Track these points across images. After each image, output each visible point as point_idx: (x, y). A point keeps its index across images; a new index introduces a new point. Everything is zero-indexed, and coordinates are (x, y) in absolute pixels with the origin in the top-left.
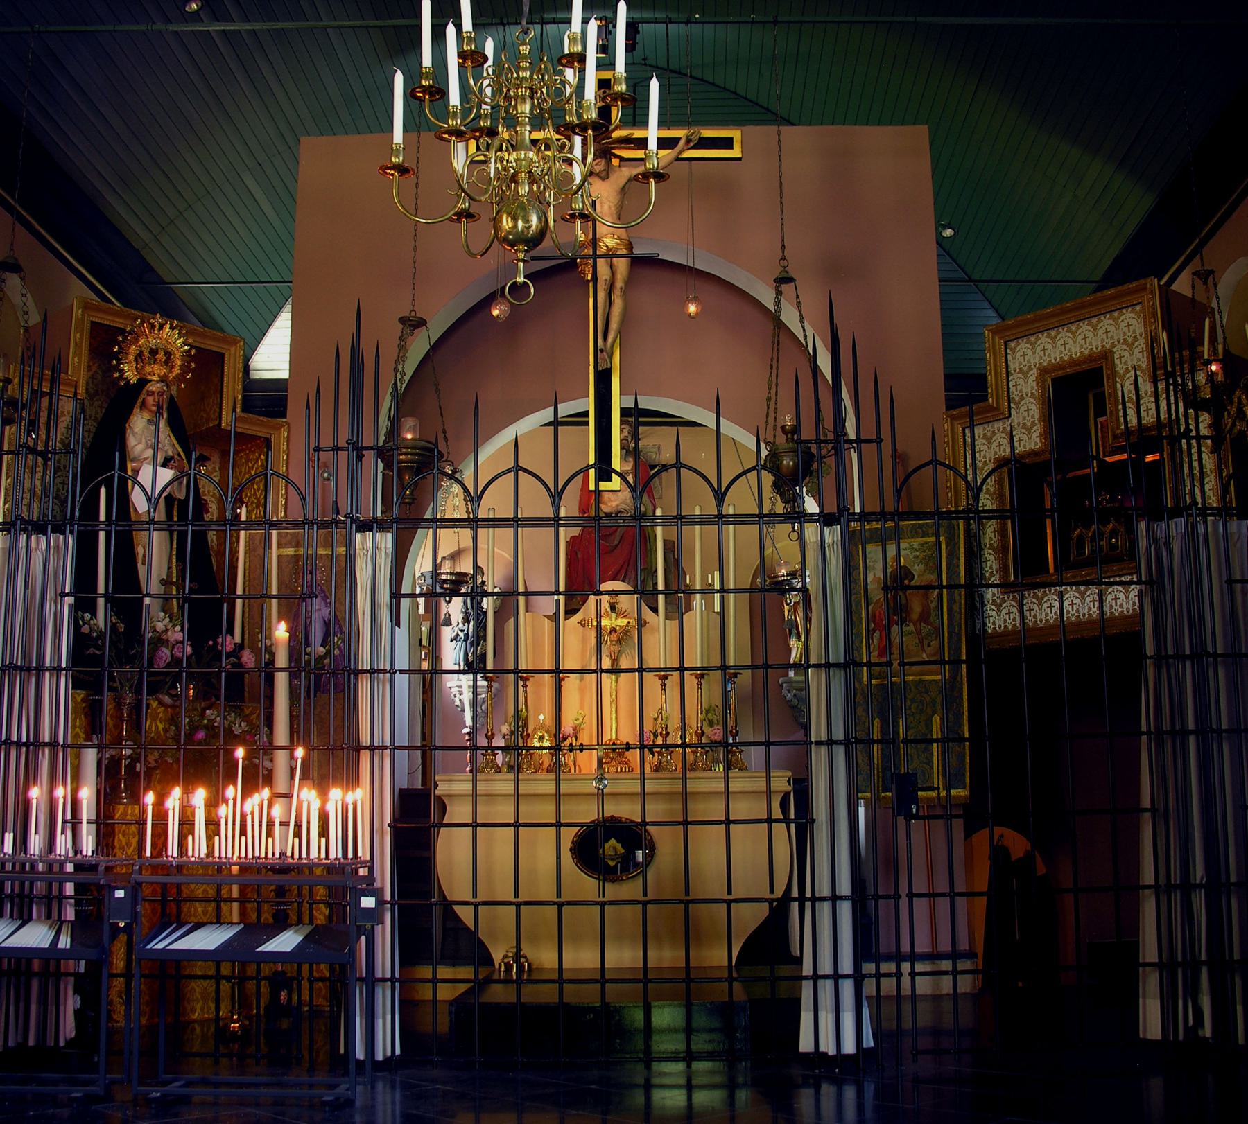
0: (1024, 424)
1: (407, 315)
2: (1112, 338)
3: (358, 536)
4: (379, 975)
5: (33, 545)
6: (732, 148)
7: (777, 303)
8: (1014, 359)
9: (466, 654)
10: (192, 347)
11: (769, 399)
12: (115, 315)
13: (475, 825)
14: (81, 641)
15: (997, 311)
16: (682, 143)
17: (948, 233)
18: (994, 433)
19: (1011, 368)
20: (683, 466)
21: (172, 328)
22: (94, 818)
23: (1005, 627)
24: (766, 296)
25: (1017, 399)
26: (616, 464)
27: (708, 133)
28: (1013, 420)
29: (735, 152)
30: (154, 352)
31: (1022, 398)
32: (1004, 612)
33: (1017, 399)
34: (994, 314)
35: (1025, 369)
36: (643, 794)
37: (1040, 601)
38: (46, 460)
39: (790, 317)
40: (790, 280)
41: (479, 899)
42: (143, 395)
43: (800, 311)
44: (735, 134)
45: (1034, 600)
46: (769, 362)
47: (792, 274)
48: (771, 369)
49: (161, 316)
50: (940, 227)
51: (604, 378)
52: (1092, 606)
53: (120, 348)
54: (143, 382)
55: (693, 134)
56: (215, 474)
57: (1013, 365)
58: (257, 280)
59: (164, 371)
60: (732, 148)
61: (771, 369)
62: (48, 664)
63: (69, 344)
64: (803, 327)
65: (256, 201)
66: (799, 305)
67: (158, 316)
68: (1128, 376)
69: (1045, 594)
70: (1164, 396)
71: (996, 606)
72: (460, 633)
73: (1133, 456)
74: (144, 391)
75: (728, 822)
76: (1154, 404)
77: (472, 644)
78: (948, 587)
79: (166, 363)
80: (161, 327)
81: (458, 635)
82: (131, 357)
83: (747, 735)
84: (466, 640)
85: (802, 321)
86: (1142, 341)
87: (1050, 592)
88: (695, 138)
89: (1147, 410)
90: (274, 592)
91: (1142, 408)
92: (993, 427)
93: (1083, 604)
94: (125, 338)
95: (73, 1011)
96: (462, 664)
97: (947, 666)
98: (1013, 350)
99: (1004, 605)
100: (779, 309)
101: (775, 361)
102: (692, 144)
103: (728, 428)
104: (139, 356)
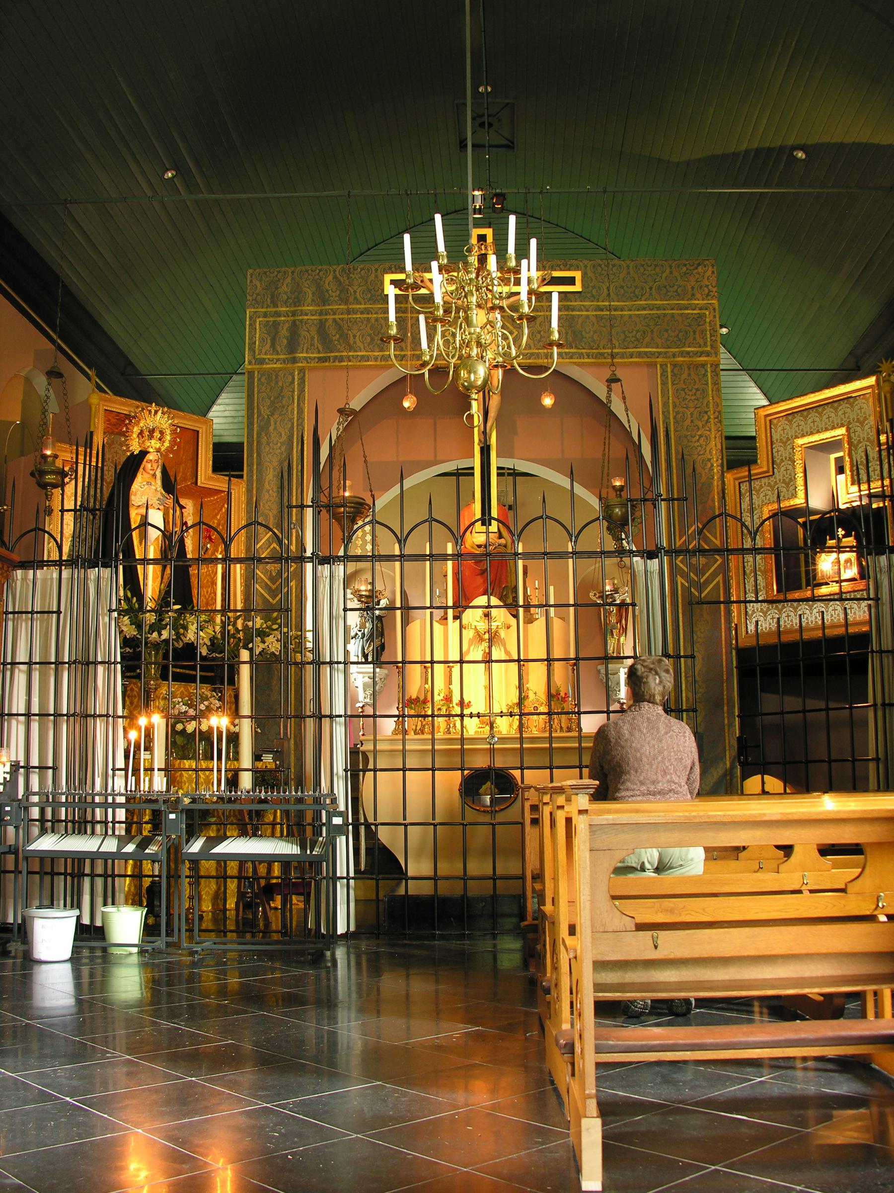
0: (784, 480)
1: (343, 407)
2: (849, 418)
3: (320, 567)
4: (338, 875)
6: (575, 285)
7: (609, 397)
8: (776, 432)
9: (363, 648)
11: (603, 466)
12: (123, 406)
13: (404, 770)
14: (551, 696)
18: (761, 487)
19: (774, 439)
20: (548, 517)
21: (163, 413)
22: (163, 767)
23: (770, 628)
24: (600, 391)
25: (778, 461)
26: (494, 513)
27: (556, 274)
28: (775, 478)
29: (578, 288)
30: (152, 432)
31: (782, 461)
32: (769, 617)
33: (778, 461)
34: (759, 391)
35: (784, 440)
36: (433, 751)
38: (94, 515)
39: (617, 407)
40: (618, 380)
42: (144, 463)
43: (625, 403)
44: (578, 275)
45: (791, 609)
46: (603, 441)
47: (619, 376)
48: (605, 445)
49: (156, 405)
51: (485, 451)
53: (127, 428)
54: (144, 453)
55: (546, 275)
56: (189, 518)
58: (207, 372)
59: (158, 445)
60: (575, 285)
61: (605, 445)
64: (627, 414)
65: (208, 312)
66: (624, 398)
67: (154, 404)
68: (860, 445)
70: (886, 461)
71: (763, 613)
72: (358, 632)
74: (145, 460)
75: (830, 761)
76: (879, 466)
77: (367, 641)
79: (160, 439)
80: (156, 412)
81: (357, 634)
82: (135, 436)
84: (362, 638)
85: (626, 410)
86: (872, 418)
89: (874, 470)
91: (870, 469)
92: (761, 482)
93: (811, 614)
94: (131, 421)
96: (360, 655)
98: (776, 425)
99: (769, 613)
100: (610, 402)
101: (607, 439)
102: (545, 282)
103: (579, 490)
104: (141, 433)
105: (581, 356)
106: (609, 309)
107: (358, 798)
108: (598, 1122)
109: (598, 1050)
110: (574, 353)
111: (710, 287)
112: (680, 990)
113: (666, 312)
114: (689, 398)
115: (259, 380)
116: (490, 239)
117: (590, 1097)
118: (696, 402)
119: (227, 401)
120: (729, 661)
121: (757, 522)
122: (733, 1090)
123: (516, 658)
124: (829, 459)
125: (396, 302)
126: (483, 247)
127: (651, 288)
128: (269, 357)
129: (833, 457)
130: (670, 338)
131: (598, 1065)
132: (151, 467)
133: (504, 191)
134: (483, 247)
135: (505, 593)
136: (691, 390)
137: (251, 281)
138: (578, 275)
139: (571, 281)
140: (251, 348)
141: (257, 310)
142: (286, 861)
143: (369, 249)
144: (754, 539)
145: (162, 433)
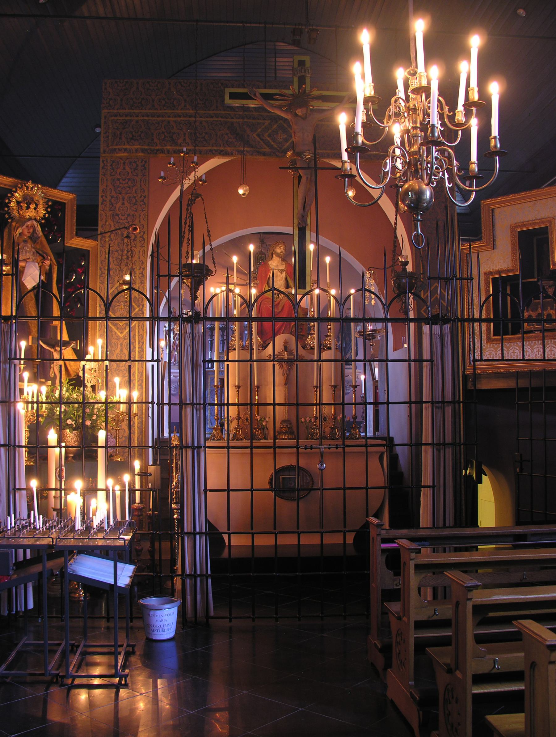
37: (532, 347)
41: (231, 531)
52: (537, 354)
53: (48, 204)
62: (412, 325)
63: (458, 337)
69: (535, 344)
73: (156, 513)
87: (551, 342)
93: (532, 352)
99: (536, 346)
111: (134, 100)
113: (228, 120)
114: (122, 186)
118: (127, 189)
123: (272, 402)
126: (303, 70)
127: (121, 100)
128: (215, 148)
130: (167, 139)
134: (303, 70)
136: (125, 180)
137: (106, 89)
139: (233, 96)
141: (110, 111)
143: (185, 68)
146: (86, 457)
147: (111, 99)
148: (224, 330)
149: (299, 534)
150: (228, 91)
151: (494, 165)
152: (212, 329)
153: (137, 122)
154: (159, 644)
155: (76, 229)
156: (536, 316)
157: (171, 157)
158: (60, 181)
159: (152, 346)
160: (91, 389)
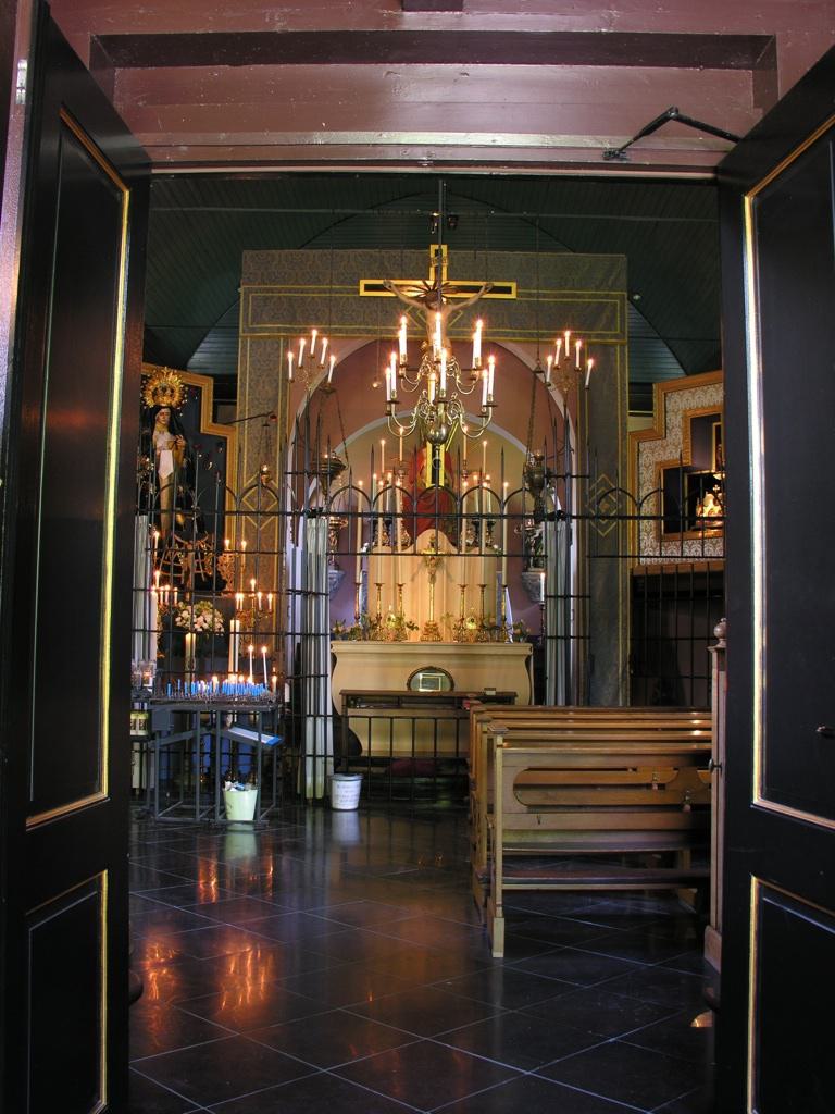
5: (308, 525)
10: (186, 385)
15: (674, 353)
16: (483, 289)
17: (637, 297)
29: (513, 296)
30: (164, 390)
50: (631, 293)
57: (669, 407)
78: (277, 634)
80: (168, 374)
83: (700, 535)
88: (490, 287)
90: (574, 513)
95: (691, 378)
97: (505, 521)
105: (514, 335)
106: (538, 296)
107: (492, 805)
108: (503, 920)
109: (504, 882)
110: (509, 333)
112: (563, 848)
115: (251, 346)
116: (445, 253)
117: (499, 906)
119: (212, 340)
120: (623, 586)
121: (643, 494)
122: (589, 909)
124: (711, 427)
125: (504, 861)
129: (715, 424)
131: (504, 892)
132: (163, 417)
133: (458, 214)
135: (490, 826)
138: (513, 285)
139: (368, 288)
140: (246, 320)
142: (426, 784)
144: (639, 510)
145: (172, 391)
146: (216, 656)
147: (354, 311)
148: (388, 524)
149: (458, 720)
150: (363, 283)
151: (748, 493)
152: (376, 523)
153: (280, 298)
154: (339, 814)
155: (214, 403)
156: (757, 104)
157: (300, 337)
158: (198, 345)
159: (295, 541)
160: (224, 578)
